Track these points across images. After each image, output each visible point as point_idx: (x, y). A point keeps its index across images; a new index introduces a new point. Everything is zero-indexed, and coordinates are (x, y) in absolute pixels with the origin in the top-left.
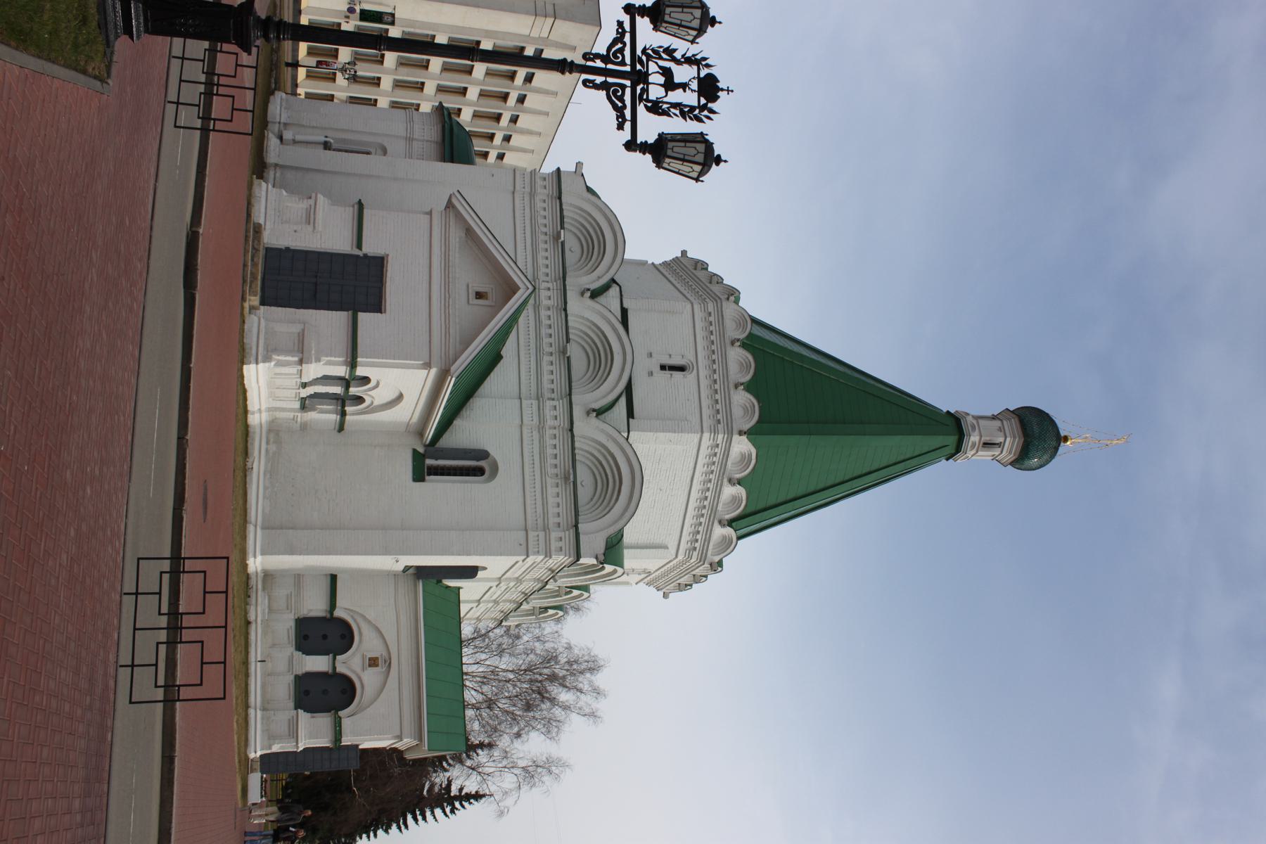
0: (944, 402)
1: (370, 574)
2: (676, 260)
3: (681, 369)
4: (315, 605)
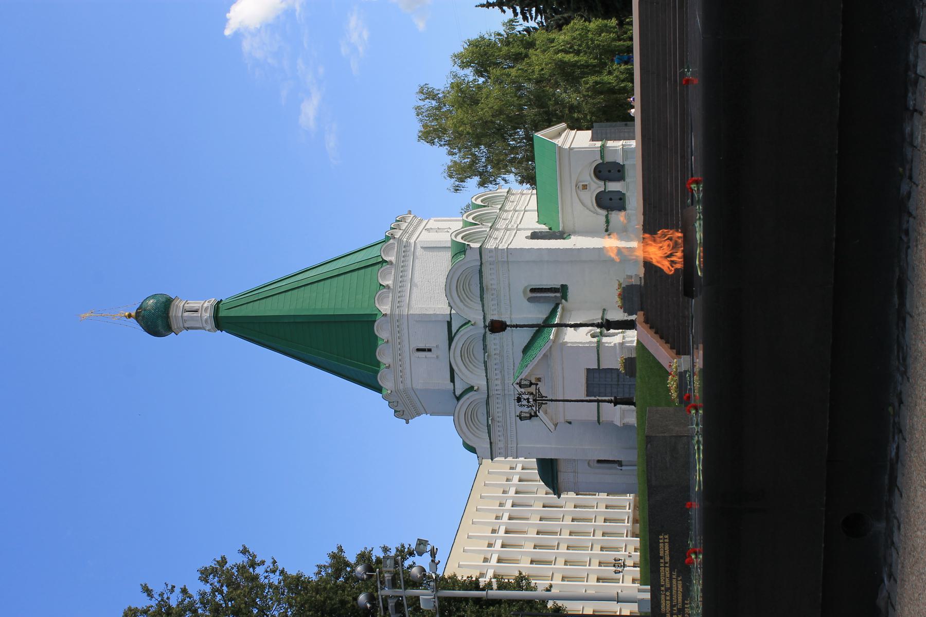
3: (418, 350)
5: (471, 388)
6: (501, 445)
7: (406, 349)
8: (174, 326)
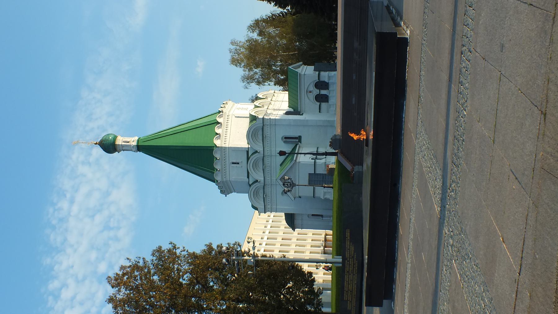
0: (141, 154)
3: (233, 163)
4: (324, 105)
5: (257, 181)
6: (269, 207)
7: (227, 163)
8: (118, 149)
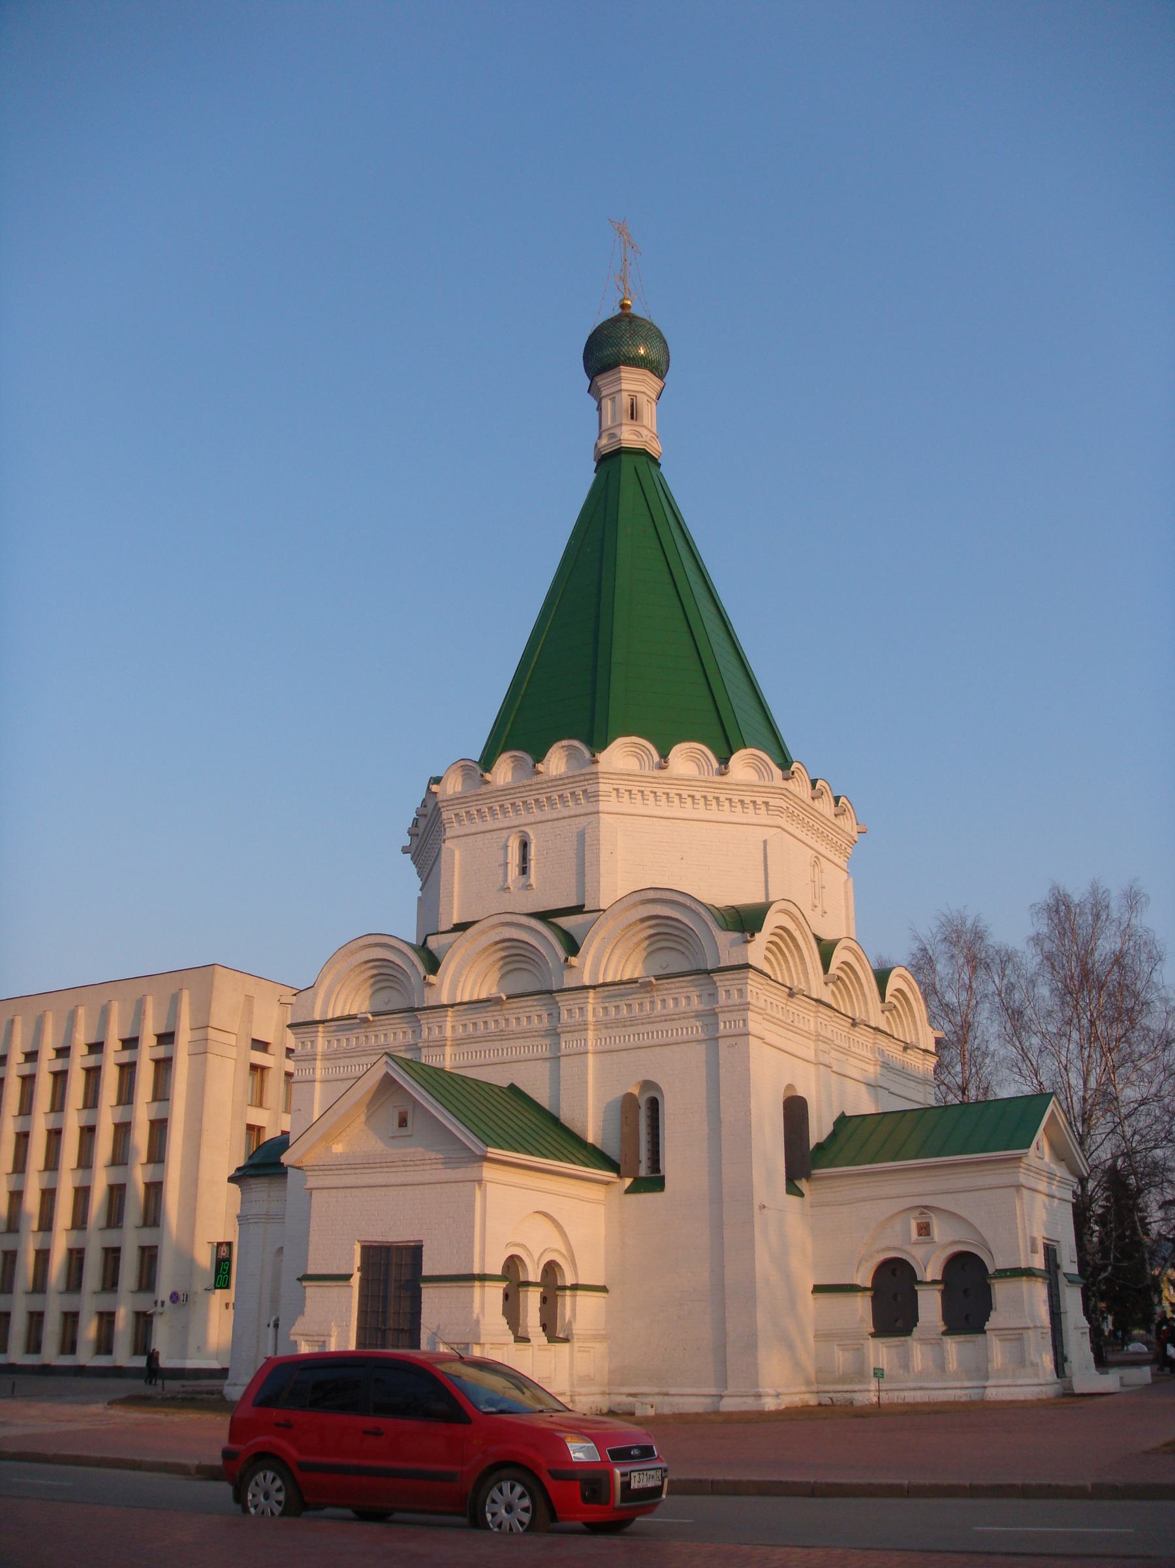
0: (585, 477)
1: (805, 1246)
2: (415, 860)
3: (525, 846)
4: (862, 1306)
7: (524, 817)
